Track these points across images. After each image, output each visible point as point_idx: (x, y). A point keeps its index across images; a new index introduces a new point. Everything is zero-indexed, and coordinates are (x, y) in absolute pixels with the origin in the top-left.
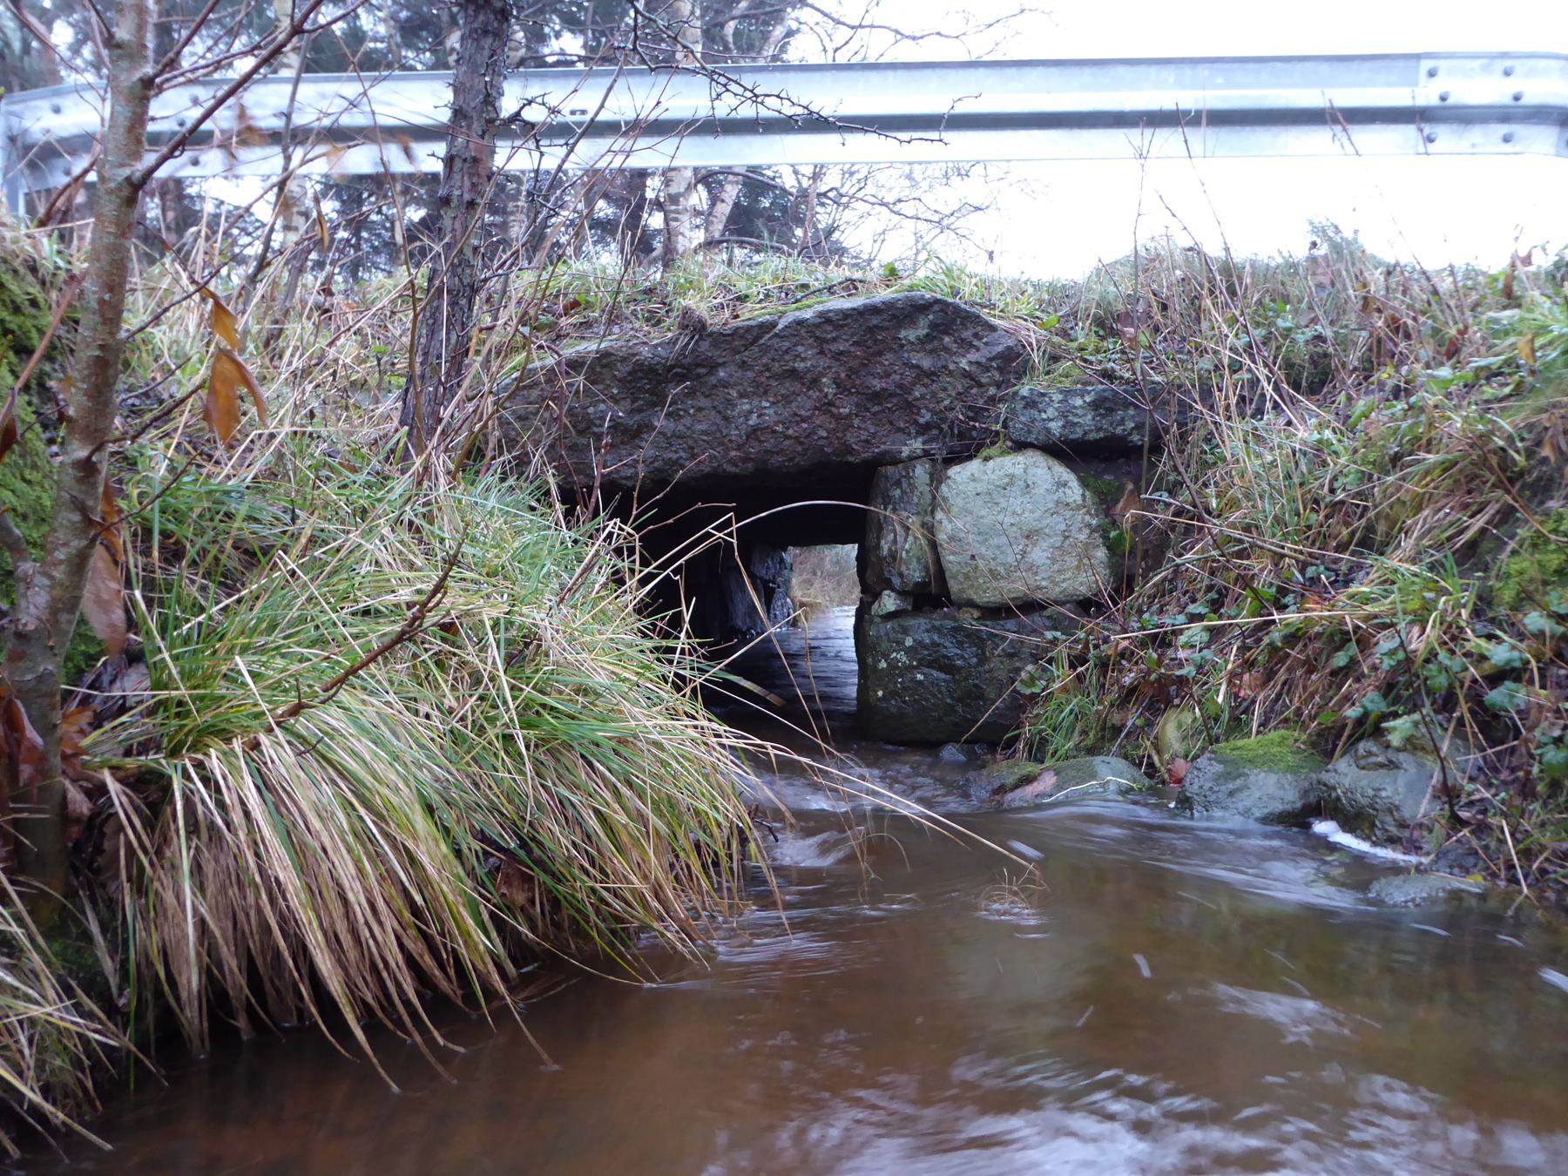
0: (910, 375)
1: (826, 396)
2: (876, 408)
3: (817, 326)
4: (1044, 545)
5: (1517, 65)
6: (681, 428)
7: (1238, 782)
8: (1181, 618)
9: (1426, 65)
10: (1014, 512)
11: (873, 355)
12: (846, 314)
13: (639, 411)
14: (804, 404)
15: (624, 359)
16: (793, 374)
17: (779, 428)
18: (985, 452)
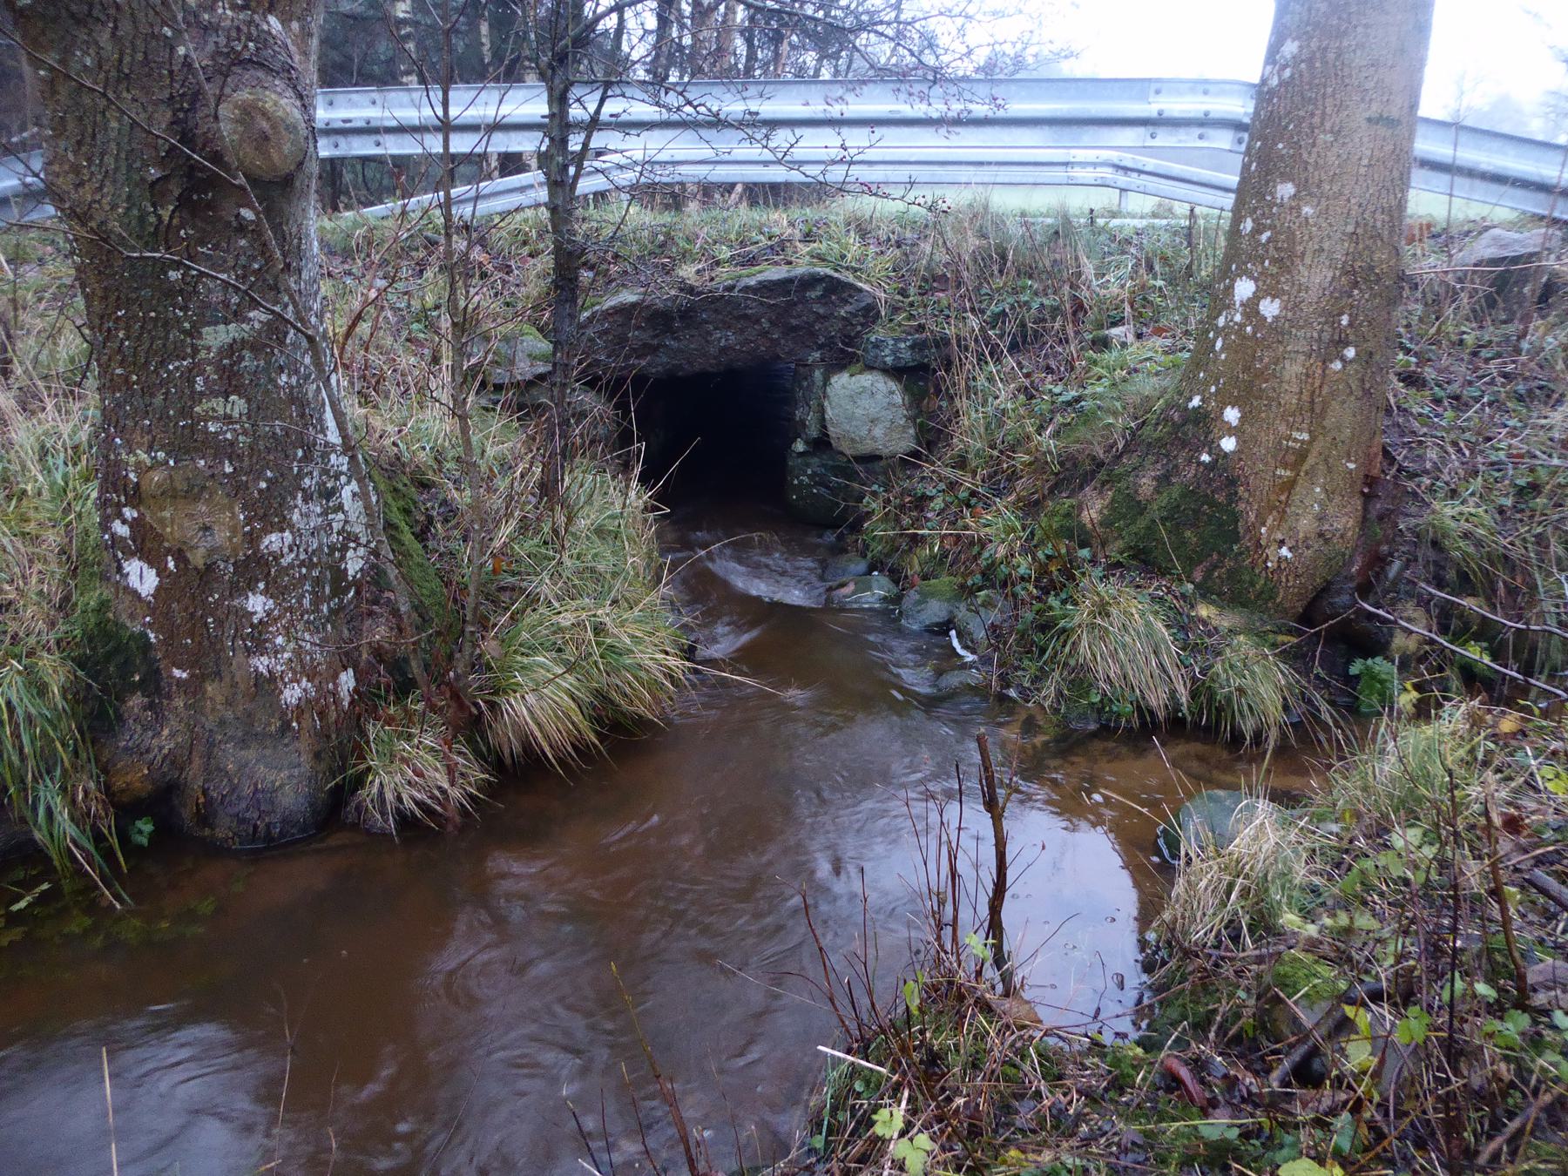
0: (812, 318)
4: (881, 426)
5: (1211, 88)
8: (934, 491)
9: (1154, 86)
13: (656, 336)
16: (746, 317)
18: (853, 368)
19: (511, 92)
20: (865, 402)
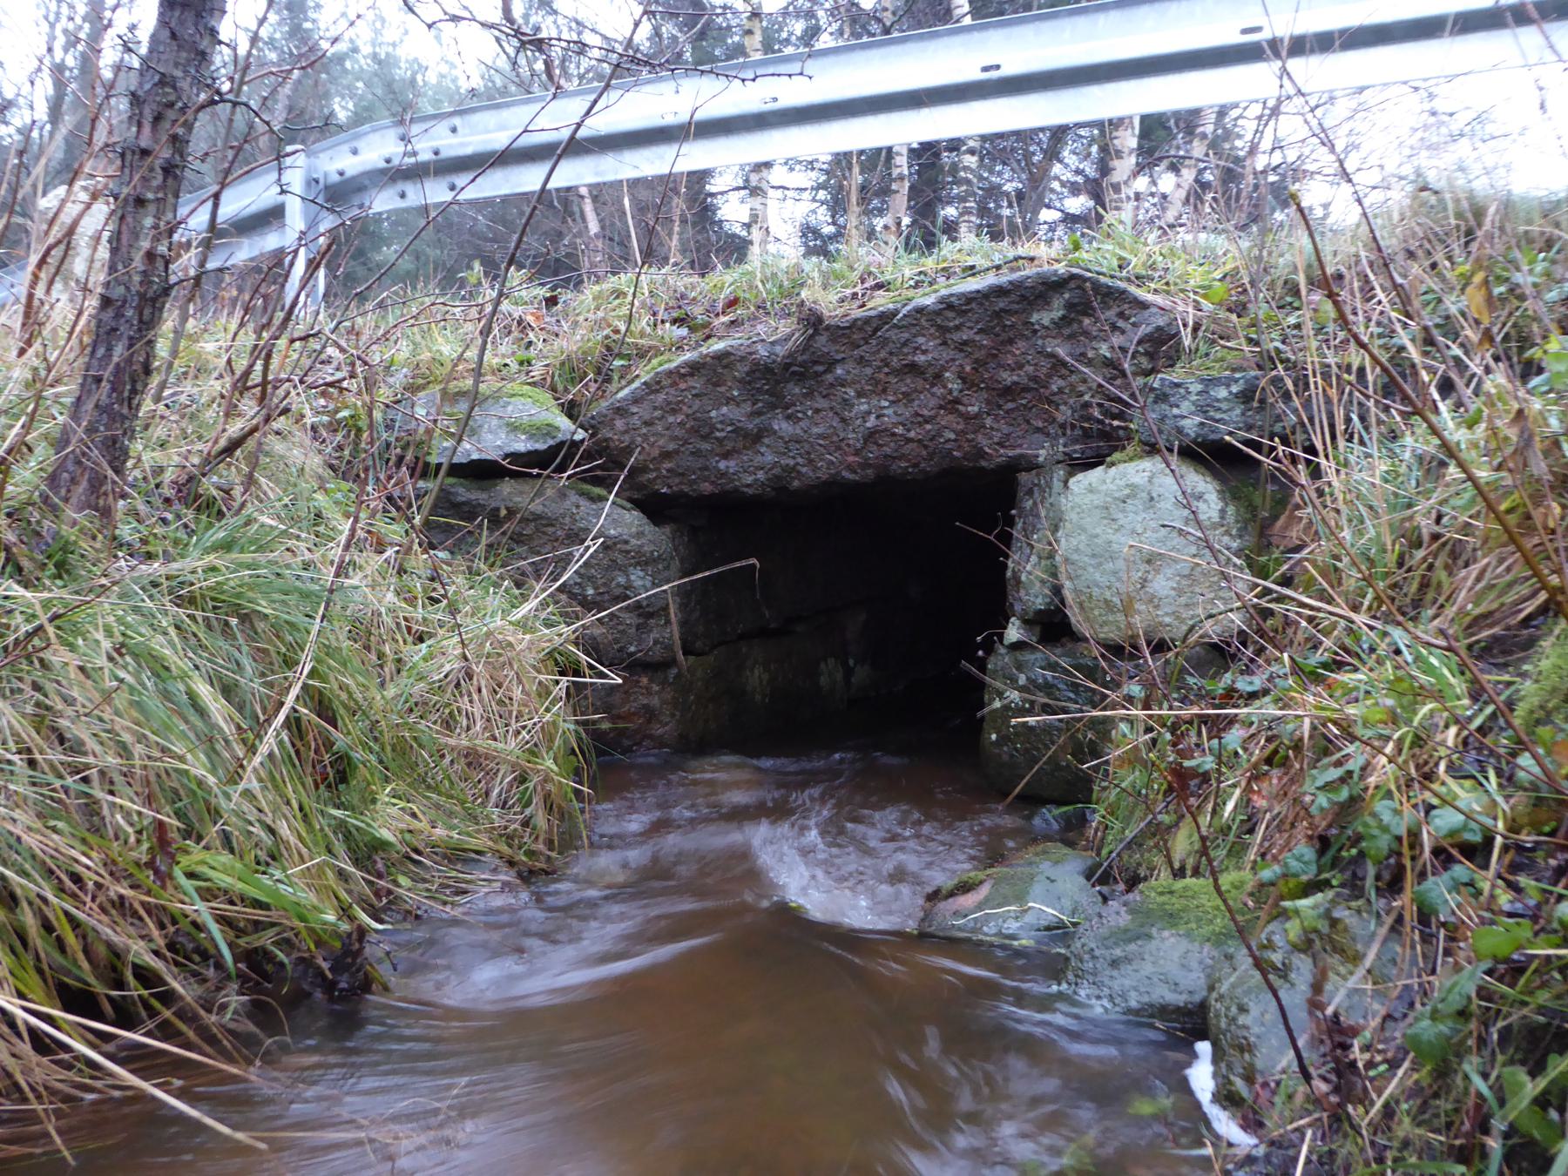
0: (1045, 364)
1: (950, 392)
2: (1010, 405)
3: (938, 313)
4: (1169, 572)
6: (798, 431)
7: (1132, 947)
10: (1133, 532)
11: (1002, 343)
12: (971, 298)
13: (759, 413)
14: (927, 403)
15: (742, 359)
16: (913, 368)
17: (899, 430)
19: (613, 95)
20: (1134, 517)
